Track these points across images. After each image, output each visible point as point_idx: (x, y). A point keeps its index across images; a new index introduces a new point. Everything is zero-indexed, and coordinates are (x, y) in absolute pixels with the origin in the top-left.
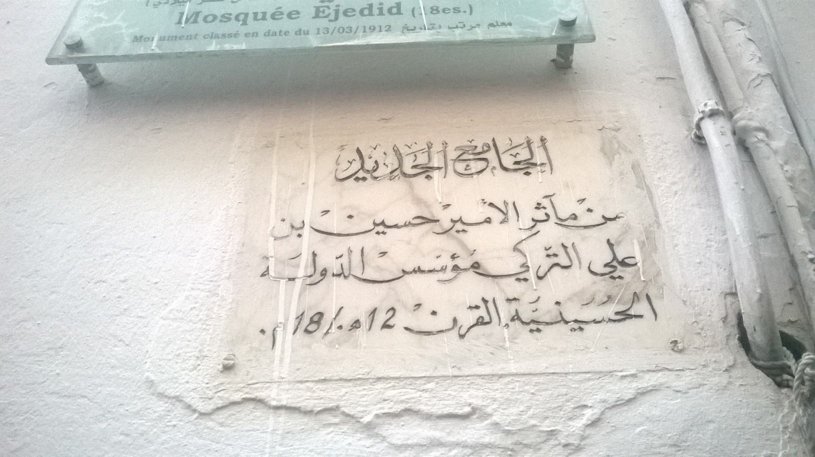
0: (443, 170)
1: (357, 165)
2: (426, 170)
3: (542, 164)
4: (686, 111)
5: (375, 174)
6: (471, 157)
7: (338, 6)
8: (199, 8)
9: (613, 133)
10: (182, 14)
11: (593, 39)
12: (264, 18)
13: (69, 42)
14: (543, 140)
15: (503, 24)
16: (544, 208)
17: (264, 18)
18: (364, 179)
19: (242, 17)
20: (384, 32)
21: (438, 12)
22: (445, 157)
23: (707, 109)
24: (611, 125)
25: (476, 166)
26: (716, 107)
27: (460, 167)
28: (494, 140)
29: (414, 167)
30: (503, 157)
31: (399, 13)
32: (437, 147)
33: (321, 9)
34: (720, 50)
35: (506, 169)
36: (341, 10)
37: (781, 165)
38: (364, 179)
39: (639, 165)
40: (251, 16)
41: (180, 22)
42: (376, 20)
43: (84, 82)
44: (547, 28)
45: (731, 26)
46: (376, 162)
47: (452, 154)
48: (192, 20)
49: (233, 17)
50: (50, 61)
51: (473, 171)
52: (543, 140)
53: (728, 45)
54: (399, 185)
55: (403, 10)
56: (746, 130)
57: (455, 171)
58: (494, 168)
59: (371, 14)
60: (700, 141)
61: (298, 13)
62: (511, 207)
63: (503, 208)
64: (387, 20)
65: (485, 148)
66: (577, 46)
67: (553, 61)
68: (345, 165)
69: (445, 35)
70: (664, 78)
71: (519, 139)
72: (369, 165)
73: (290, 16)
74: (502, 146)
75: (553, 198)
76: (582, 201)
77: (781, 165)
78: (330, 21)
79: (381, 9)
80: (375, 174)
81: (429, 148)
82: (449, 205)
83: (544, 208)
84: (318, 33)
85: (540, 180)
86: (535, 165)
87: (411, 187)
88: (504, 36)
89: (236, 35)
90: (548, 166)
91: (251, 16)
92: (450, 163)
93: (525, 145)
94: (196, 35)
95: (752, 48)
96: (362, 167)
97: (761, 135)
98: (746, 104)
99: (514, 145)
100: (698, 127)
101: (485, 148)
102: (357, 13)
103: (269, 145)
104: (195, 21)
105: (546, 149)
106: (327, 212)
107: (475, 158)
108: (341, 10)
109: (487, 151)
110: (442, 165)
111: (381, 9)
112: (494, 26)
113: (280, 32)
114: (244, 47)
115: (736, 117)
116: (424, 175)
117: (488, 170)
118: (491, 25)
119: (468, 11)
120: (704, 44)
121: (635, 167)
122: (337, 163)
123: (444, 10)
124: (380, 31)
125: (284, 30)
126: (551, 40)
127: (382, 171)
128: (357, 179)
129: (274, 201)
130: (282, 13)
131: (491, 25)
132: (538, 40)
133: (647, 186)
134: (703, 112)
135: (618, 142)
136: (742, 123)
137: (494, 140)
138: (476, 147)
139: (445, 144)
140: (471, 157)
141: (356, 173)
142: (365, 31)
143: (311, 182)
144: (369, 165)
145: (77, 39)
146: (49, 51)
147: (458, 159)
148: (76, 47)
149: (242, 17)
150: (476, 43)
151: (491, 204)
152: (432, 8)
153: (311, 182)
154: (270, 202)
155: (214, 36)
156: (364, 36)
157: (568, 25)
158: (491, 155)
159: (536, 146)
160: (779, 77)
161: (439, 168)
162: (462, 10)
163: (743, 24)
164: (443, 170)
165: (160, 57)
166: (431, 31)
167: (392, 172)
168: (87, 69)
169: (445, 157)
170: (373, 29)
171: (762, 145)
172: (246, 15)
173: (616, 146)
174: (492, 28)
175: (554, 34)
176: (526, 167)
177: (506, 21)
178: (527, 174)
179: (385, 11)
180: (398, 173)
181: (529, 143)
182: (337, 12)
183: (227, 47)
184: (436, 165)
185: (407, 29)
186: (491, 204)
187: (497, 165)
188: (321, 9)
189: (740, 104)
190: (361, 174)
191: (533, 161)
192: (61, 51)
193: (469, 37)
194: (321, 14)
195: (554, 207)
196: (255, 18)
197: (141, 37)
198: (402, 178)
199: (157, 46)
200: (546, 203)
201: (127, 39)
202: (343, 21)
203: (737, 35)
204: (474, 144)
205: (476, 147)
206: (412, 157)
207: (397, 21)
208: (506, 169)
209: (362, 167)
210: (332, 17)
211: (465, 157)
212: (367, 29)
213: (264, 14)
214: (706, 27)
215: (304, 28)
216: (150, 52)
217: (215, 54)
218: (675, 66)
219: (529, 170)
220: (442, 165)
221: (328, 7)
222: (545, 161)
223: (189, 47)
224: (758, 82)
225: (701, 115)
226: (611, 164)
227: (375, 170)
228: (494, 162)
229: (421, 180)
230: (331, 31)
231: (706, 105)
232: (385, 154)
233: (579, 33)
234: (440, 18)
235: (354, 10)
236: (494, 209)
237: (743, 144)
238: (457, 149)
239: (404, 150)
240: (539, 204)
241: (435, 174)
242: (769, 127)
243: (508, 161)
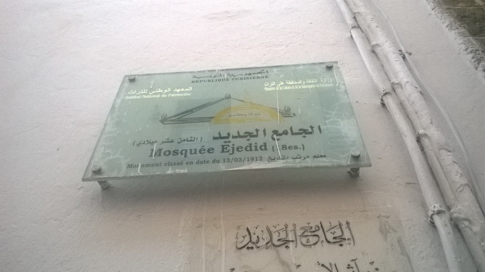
0: (295, 242)
1: (247, 239)
2: (285, 242)
3: (349, 239)
4: (424, 205)
5: (258, 245)
6: (310, 234)
7: (233, 145)
8: (161, 147)
9: (385, 219)
10: (153, 150)
11: (370, 165)
12: (195, 153)
13: (94, 169)
14: (348, 223)
15: (321, 156)
16: (352, 268)
17: (195, 153)
18: (252, 248)
19: (184, 152)
20: (258, 162)
21: (286, 149)
22: (295, 234)
23: (436, 210)
24: (384, 214)
25: (313, 240)
26: (440, 209)
27: (304, 240)
28: (321, 223)
29: (279, 240)
30: (326, 234)
31: (266, 149)
32: (291, 227)
33: (225, 147)
34: (439, 167)
35: (329, 242)
36: (236, 147)
37: (480, 242)
38: (252, 248)
39: (401, 240)
40: (189, 152)
41: (151, 156)
42: (254, 154)
43: (99, 186)
44: (346, 161)
45: (444, 152)
46: (258, 237)
47: (299, 232)
48: (158, 154)
49: (179, 152)
50: (84, 180)
51: (311, 243)
52: (348, 223)
53: (443, 164)
54: (271, 252)
55: (267, 147)
56: (457, 219)
57: (302, 243)
58: (322, 241)
59: (251, 150)
60: (433, 224)
61: (213, 149)
62: (334, 267)
63: (329, 267)
64: (259, 153)
65: (317, 228)
66: (360, 169)
67: (349, 172)
68: (241, 239)
69: (290, 163)
70: (409, 183)
71: (335, 223)
72: (254, 239)
73: (209, 151)
74: (326, 226)
75: (356, 261)
76: (372, 263)
77: (480, 242)
78: (230, 154)
79: (256, 147)
80: (258, 245)
81: (286, 228)
82: (299, 265)
83: (352, 268)
84: (224, 162)
85: (348, 250)
86: (345, 239)
87: (278, 253)
88: (322, 164)
89: (181, 164)
90: (352, 240)
91: (189, 152)
92: (298, 238)
93: (338, 227)
94: (160, 164)
95: (456, 167)
96: (251, 241)
97: (466, 223)
98: (456, 203)
99: (332, 226)
100: (432, 218)
101: (317, 228)
102: (244, 149)
103: (200, 226)
104: (160, 155)
105: (350, 229)
106: (233, 269)
107: (313, 234)
108: (236, 147)
109: (318, 230)
110: (294, 239)
111: (256, 147)
112: (317, 157)
113: (204, 161)
114: (186, 171)
115: (452, 211)
116: (284, 246)
117: (319, 243)
118: (315, 157)
119: (302, 148)
120: (430, 163)
121: (399, 241)
122: (237, 238)
123: (289, 148)
124: (257, 160)
125: (206, 160)
126: (348, 166)
127: (262, 243)
128: (248, 248)
129: (204, 263)
130: (205, 150)
131: (315, 157)
132: (340, 166)
133: (407, 254)
134: (433, 211)
135: (389, 225)
136: (455, 215)
137: (321, 223)
138: (312, 227)
139: (294, 225)
140: (310, 234)
141: (247, 244)
142: (248, 161)
143: (223, 250)
144: (254, 239)
145: (98, 168)
146: (83, 174)
147: (303, 235)
148: (98, 172)
149: (184, 152)
150: (307, 167)
151: (323, 265)
152: (283, 146)
153: (223, 250)
154: (202, 263)
155: (170, 164)
156: (249, 164)
157: (356, 158)
158: (320, 233)
159: (344, 226)
160: (473, 186)
161: (292, 241)
162: (299, 147)
163: (450, 152)
164: (295, 242)
165: (142, 177)
166: (284, 161)
167: (267, 244)
168: (102, 182)
169: (295, 234)
170: (253, 159)
171: (467, 229)
172: (186, 151)
173: (388, 227)
174: (315, 159)
175: (349, 163)
176: (340, 241)
177: (323, 155)
178: (341, 245)
179: (258, 148)
180: (270, 244)
181: (340, 225)
182: (233, 148)
183: (177, 171)
184: (291, 239)
185: (271, 159)
186: (323, 265)
187: (324, 239)
188: (225, 147)
189: (453, 202)
190: (250, 245)
191: (343, 237)
192: (90, 174)
193: (304, 164)
194: (225, 150)
195: (357, 267)
196: (191, 153)
197: (132, 165)
198: (272, 247)
199: (140, 171)
200: (352, 264)
201: (124, 167)
202: (237, 155)
203: (448, 158)
204: (310, 225)
205: (312, 227)
206: (277, 234)
207: (265, 154)
208: (329, 242)
209: (251, 241)
210: (231, 152)
211: (306, 234)
212: (250, 159)
213: (196, 150)
214: (430, 153)
215: (217, 159)
216: (137, 175)
217: (171, 175)
218: (414, 174)
219: (342, 243)
220: (294, 239)
221: (228, 146)
222: (350, 237)
223: (157, 171)
224: (461, 189)
225: (432, 213)
226: (386, 240)
227: (258, 242)
228: (322, 238)
229: (282, 249)
230: (231, 160)
231: (434, 207)
232: (262, 231)
233: (364, 162)
234: (287, 152)
235: (242, 148)
236: (325, 269)
237: (456, 226)
238: (301, 228)
239: (272, 229)
240: (349, 265)
241: (291, 245)
242: (471, 218)
243: (330, 237)
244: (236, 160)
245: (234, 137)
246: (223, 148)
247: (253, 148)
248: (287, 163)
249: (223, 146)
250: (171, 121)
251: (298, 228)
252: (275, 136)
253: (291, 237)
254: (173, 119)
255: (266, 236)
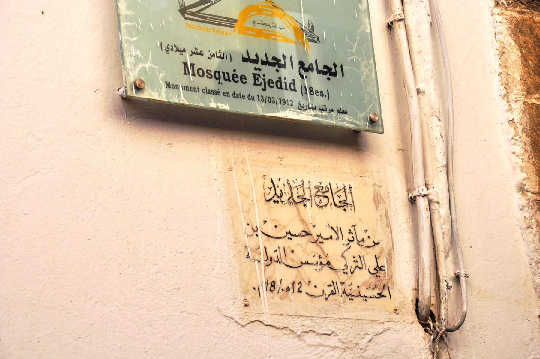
1: (273, 192)
25: (324, 201)
35: (336, 205)
47: (314, 191)
68: (268, 191)
72: (279, 193)
144: (279, 193)
159: (348, 190)
185: (302, 108)
190: (276, 198)
208: (336, 205)
210: (263, 86)
228: (331, 201)
239: (293, 185)
244: (271, 100)
245: (263, 63)
246: (255, 80)
247: (284, 86)
248: (316, 115)
249: (254, 75)
250: (192, 14)
251: (312, 186)
252: (304, 74)
253: (307, 196)
254: (194, 10)
255: (287, 190)
